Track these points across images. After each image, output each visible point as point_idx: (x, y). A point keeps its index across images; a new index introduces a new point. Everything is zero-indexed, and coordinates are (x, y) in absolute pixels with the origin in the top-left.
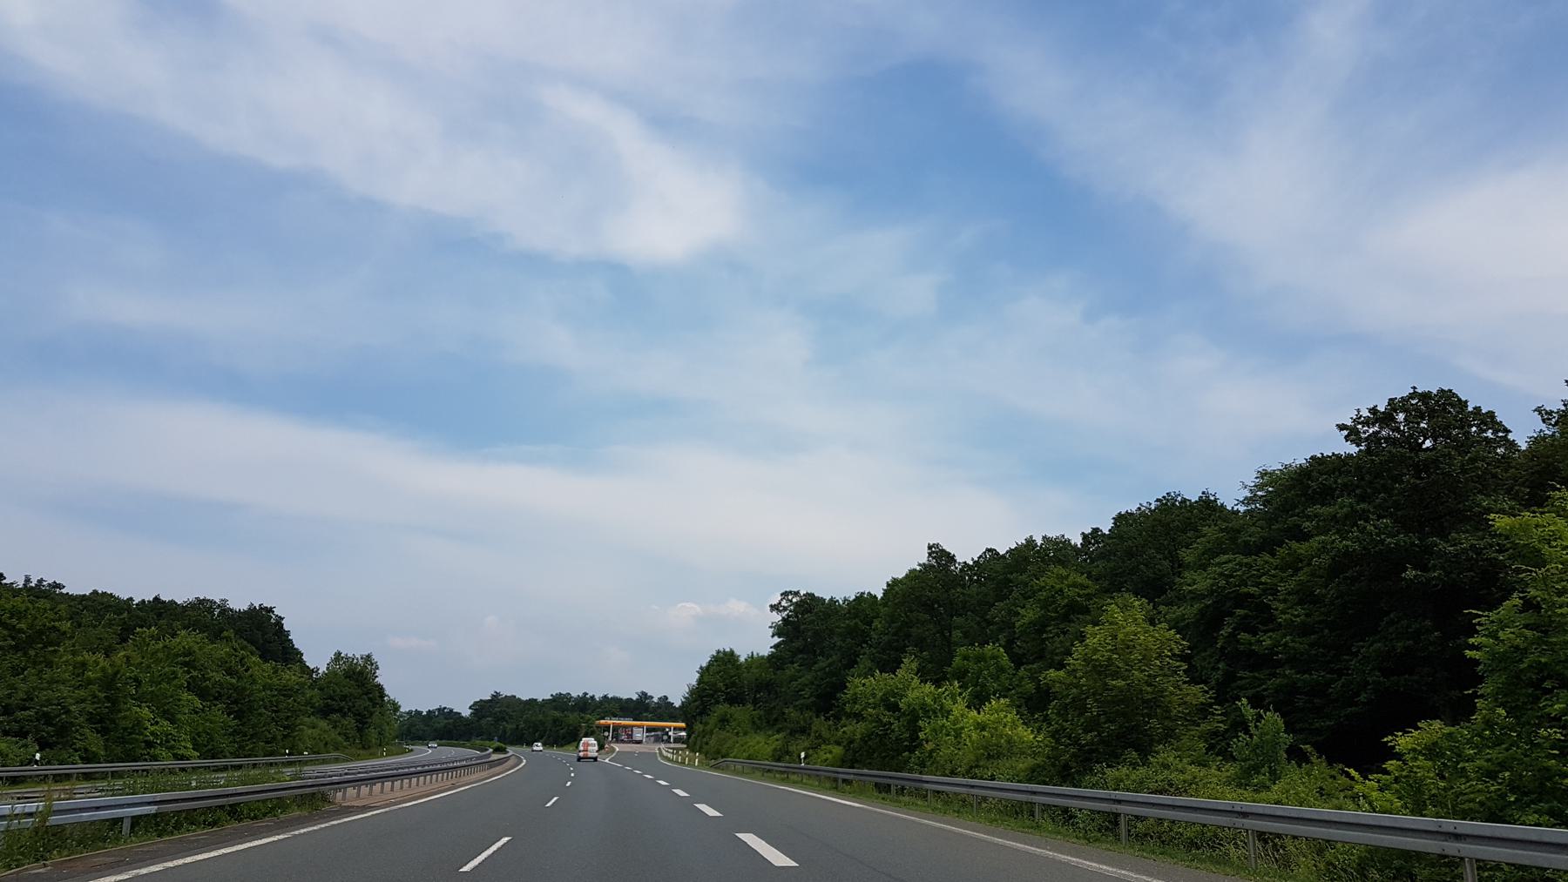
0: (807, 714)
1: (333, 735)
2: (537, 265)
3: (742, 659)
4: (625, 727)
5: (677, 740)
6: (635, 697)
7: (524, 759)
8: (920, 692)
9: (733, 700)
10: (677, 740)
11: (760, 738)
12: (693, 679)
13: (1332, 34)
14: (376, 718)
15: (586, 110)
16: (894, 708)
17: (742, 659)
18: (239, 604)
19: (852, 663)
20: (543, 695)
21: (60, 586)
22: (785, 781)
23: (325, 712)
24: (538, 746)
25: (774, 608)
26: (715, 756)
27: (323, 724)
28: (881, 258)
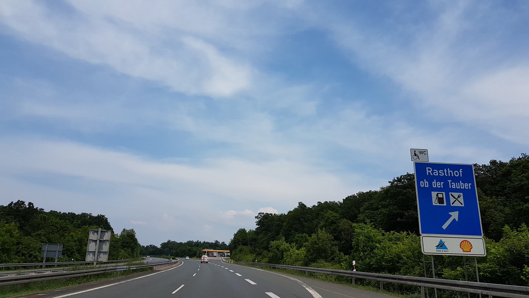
0: (262, 250)
1: (126, 254)
2: (181, 97)
3: (247, 231)
4: (211, 252)
5: (227, 256)
6: (214, 242)
7: (183, 262)
8: (285, 245)
9: (244, 244)
10: (227, 256)
11: (250, 256)
12: (232, 237)
13: (450, 22)
14: (135, 249)
15: (198, 45)
16: (278, 249)
17: (247, 231)
18: (95, 214)
19: (278, 234)
20: (184, 241)
21: (43, 209)
22: (252, 267)
23: (124, 247)
24: (187, 258)
25: (256, 217)
26: (237, 261)
27: (123, 251)
28: (297, 96)
